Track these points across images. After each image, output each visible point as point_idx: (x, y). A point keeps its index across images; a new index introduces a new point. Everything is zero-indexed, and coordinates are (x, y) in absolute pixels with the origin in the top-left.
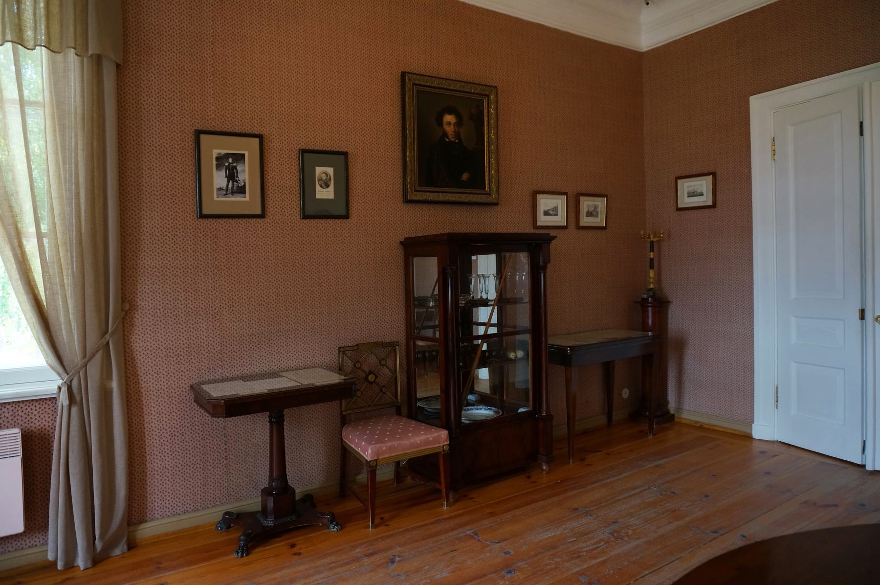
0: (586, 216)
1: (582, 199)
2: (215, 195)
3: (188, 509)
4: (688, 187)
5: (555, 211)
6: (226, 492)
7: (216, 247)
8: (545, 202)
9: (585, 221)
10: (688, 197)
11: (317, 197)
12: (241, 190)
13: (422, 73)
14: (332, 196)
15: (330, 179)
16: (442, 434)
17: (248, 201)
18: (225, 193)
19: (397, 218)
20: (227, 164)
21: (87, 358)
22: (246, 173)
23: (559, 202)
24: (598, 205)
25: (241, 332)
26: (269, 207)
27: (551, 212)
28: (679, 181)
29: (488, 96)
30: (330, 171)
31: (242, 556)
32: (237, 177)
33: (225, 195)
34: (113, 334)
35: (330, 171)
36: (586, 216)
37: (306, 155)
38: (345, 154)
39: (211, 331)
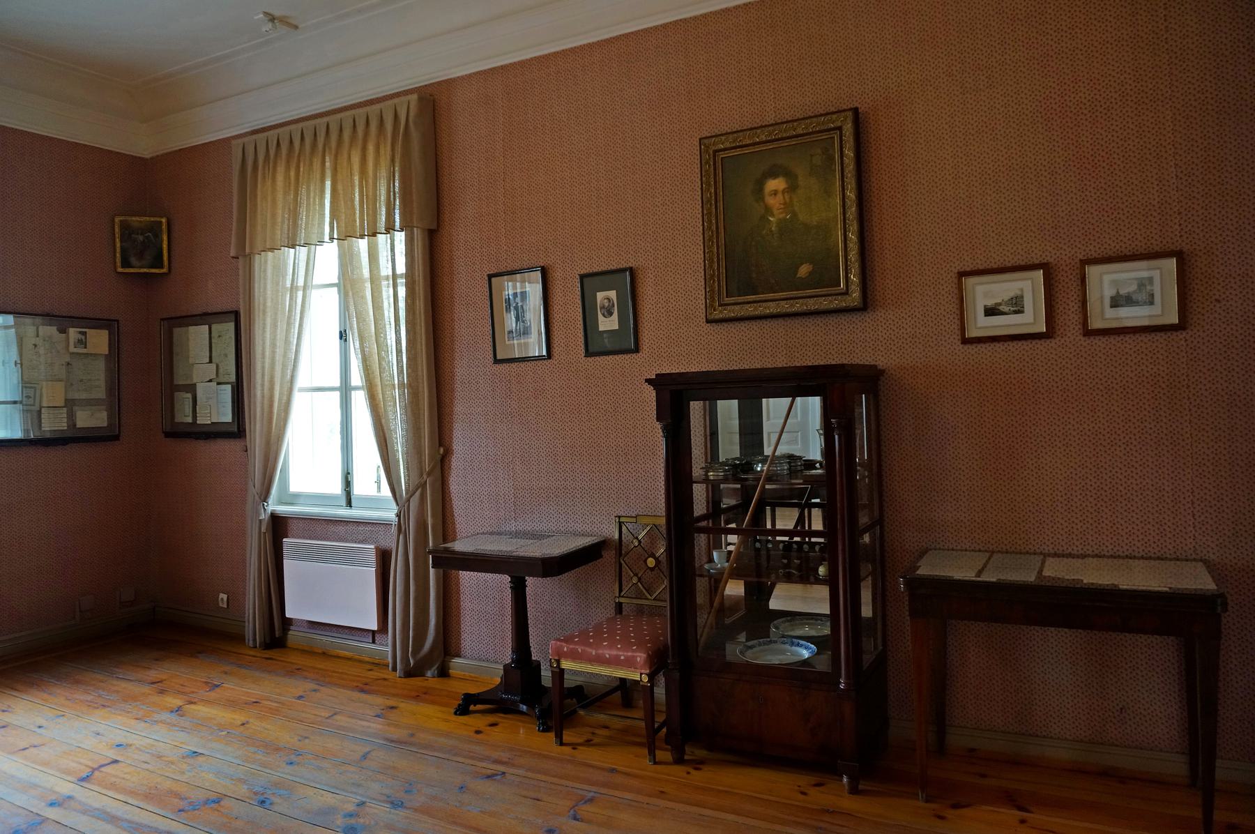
0: (1112, 307)
1: (1093, 271)
2: (507, 339)
5: (1017, 305)
11: (617, 328)
13: (799, 116)
16: (637, 657)
21: (411, 494)
27: (1004, 308)
29: (840, 128)
30: (612, 294)
34: (429, 474)
35: (612, 294)
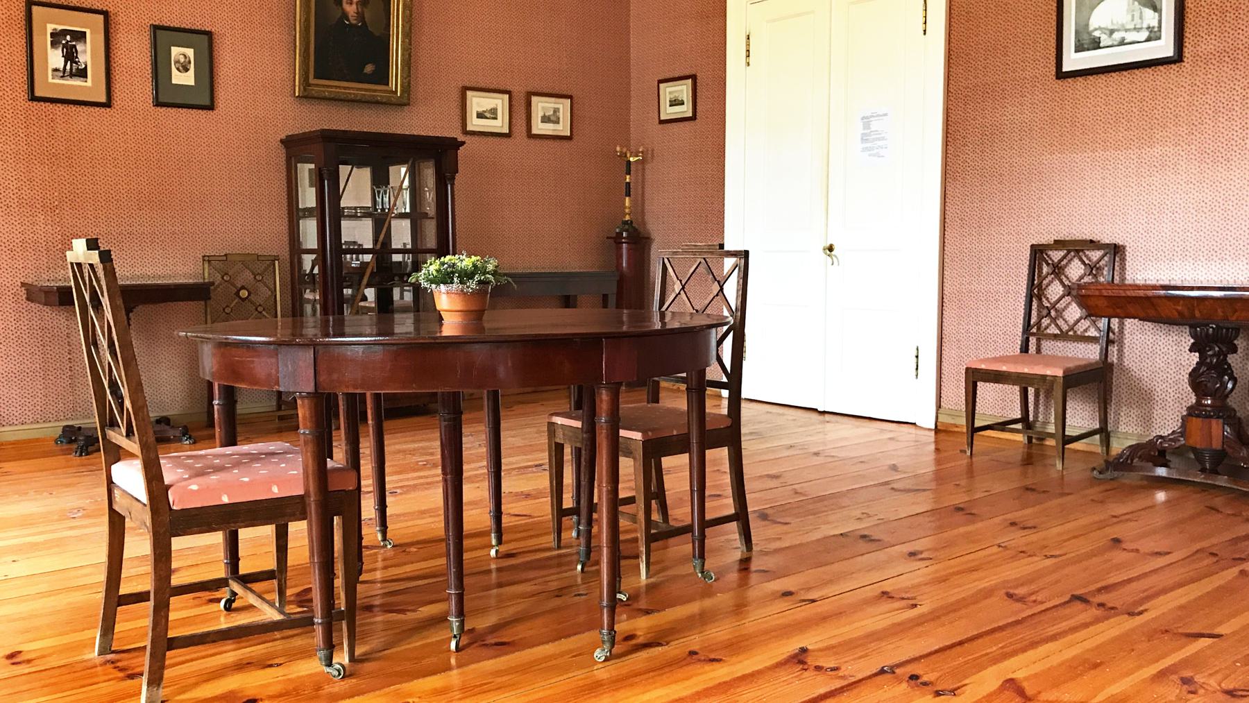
0: (542, 122)
1: (534, 99)
3: (27, 420)
4: (670, 93)
5: (493, 114)
6: (71, 406)
7: (52, 132)
8: (478, 102)
9: (539, 128)
10: (670, 106)
12: (82, 74)
14: (192, 83)
15: (190, 62)
17: (91, 87)
18: (62, 74)
19: (276, 112)
20: (64, 42)
22: (88, 54)
23: (499, 102)
24: (558, 109)
25: (86, 231)
26: (116, 91)
27: (488, 115)
28: (662, 86)
30: (190, 52)
31: (81, 455)
32: (77, 57)
33: (62, 77)
35: (190, 52)
36: (542, 122)
37: (159, 32)
38: (209, 34)
39: (50, 226)
